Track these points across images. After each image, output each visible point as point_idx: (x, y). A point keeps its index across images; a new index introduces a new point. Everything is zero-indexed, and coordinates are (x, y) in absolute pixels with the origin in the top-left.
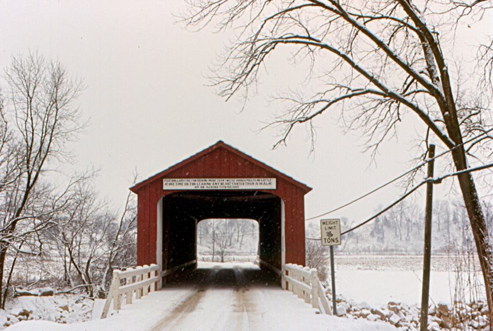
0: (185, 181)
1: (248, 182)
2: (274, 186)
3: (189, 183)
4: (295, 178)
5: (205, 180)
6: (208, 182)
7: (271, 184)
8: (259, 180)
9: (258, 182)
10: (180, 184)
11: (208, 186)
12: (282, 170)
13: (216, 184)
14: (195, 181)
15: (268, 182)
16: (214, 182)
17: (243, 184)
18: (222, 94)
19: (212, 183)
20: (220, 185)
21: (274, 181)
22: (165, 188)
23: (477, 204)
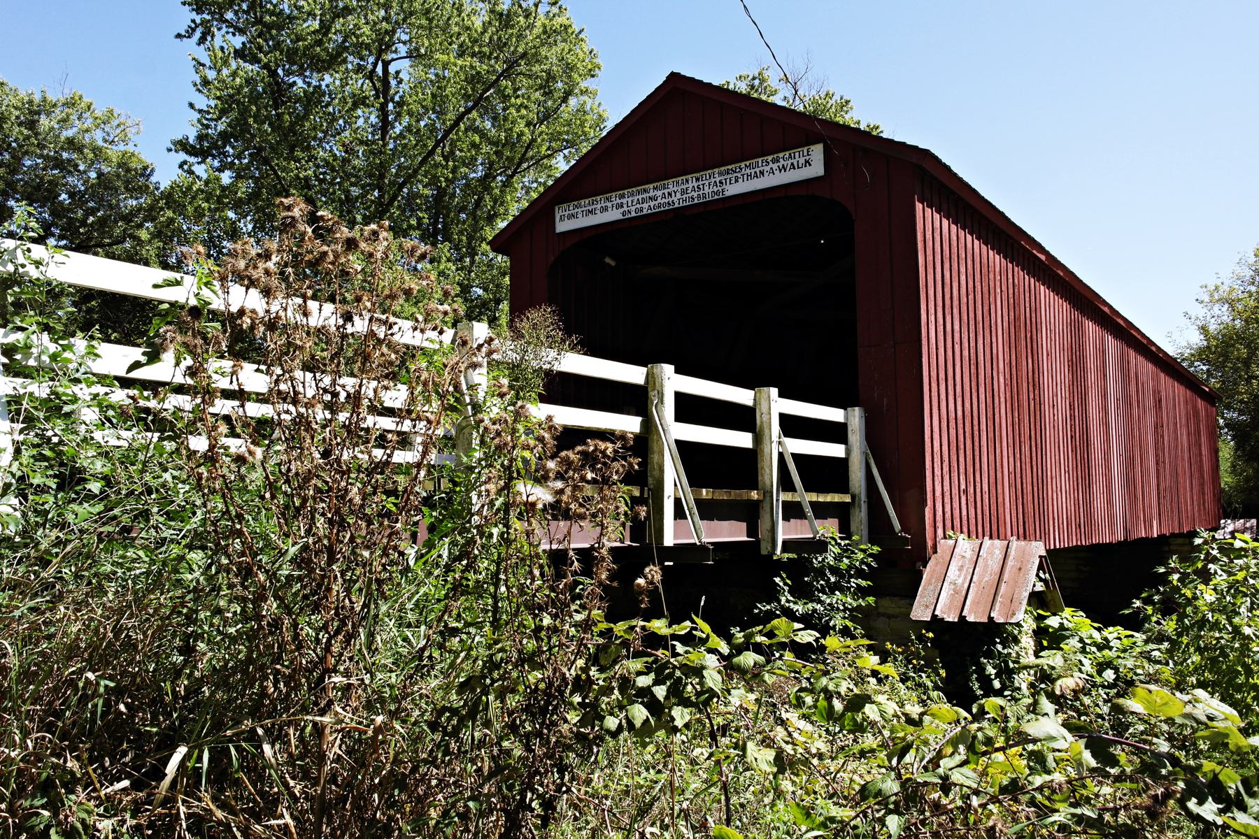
0: (600, 202)
1: (748, 171)
2: (817, 168)
3: (609, 204)
4: (891, 132)
5: (645, 191)
6: (652, 194)
7: (811, 164)
8: (776, 161)
9: (775, 166)
10: (591, 212)
11: (652, 204)
12: (1053, 253)
13: (670, 194)
14: (622, 196)
15: (802, 161)
16: (666, 191)
17: (762, 173)
18: (847, 102)
19: (659, 193)
20: (678, 195)
21: (817, 152)
22: (562, 226)
23: (227, 104)
